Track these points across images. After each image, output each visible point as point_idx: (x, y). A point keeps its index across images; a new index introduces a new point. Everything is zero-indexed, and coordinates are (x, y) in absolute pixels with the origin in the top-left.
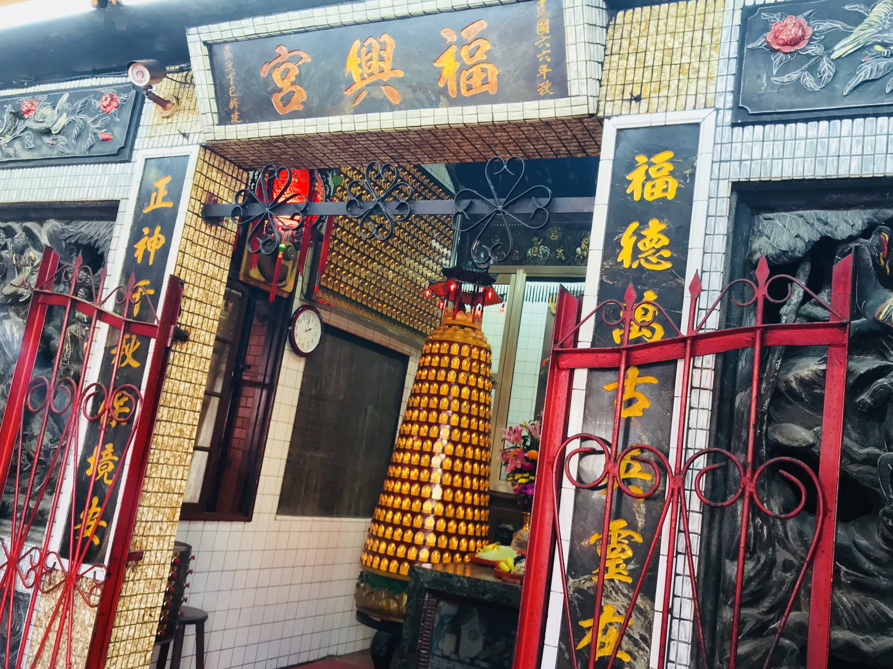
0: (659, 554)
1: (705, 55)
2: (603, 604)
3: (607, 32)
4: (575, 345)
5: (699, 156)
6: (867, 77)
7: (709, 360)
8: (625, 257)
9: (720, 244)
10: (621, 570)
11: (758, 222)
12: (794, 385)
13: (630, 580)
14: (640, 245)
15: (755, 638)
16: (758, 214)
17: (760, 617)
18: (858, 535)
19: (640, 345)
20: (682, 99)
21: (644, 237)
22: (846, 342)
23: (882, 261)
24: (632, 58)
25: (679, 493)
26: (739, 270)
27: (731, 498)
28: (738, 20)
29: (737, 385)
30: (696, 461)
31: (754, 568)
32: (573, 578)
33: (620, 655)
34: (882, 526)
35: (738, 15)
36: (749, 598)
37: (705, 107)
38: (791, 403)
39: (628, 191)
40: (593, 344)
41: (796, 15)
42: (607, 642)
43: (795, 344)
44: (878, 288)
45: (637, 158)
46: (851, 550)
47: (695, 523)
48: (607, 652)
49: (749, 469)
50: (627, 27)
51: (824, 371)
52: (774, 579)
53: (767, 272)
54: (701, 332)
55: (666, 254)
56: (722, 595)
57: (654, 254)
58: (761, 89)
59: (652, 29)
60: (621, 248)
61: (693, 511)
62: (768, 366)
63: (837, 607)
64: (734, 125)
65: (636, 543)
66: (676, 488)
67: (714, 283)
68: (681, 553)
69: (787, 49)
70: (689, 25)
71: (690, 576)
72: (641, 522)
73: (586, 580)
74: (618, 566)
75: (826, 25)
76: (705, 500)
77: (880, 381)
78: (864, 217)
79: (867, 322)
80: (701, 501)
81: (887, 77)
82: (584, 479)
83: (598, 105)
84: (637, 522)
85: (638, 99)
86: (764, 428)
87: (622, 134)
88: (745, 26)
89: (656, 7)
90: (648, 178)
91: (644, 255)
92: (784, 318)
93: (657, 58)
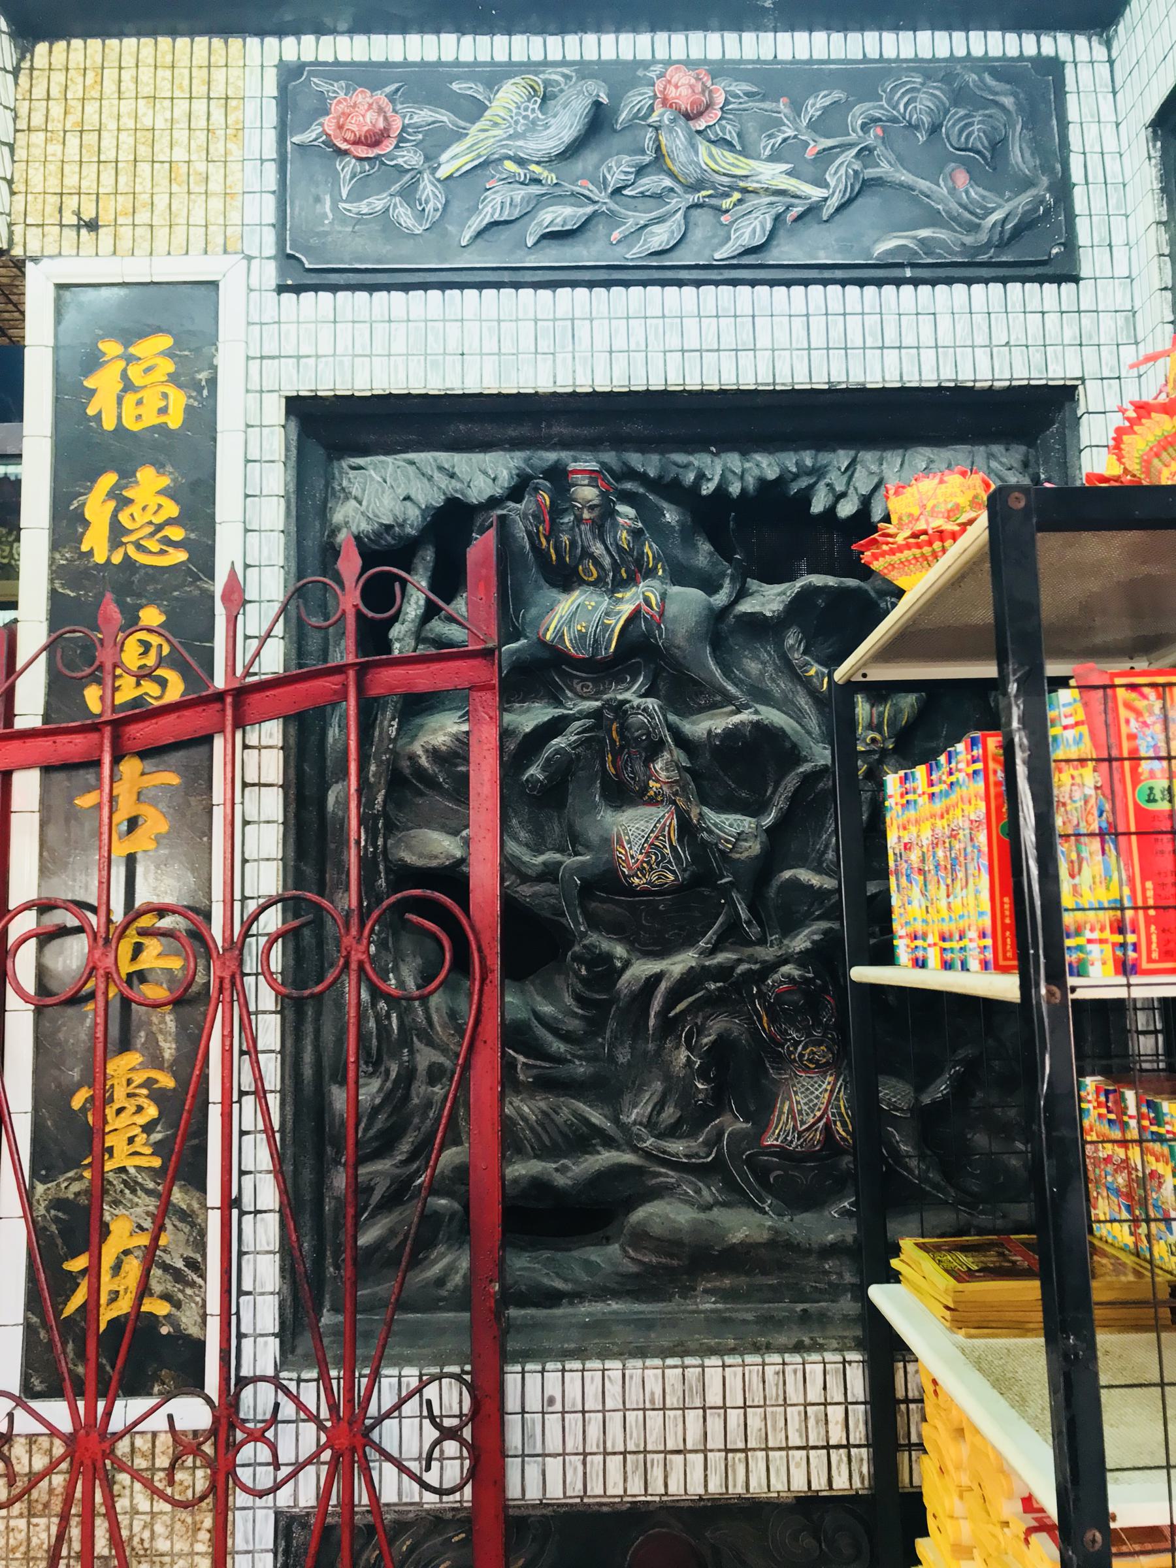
0: (207, 1103)
1: (217, 150)
2: (107, 1217)
3: (16, 84)
4: (9, 722)
5: (220, 345)
6: (496, 217)
7: (272, 732)
8: (96, 542)
9: (273, 514)
10: (138, 1146)
11: (341, 473)
12: (424, 761)
13: (156, 1162)
14: (124, 518)
15: (390, 1211)
16: (339, 459)
17: (398, 1171)
18: (539, 999)
19: (140, 712)
20: (180, 232)
21: (129, 502)
22: (495, 681)
23: (544, 543)
24: (73, 140)
25: (233, 984)
26: (313, 561)
27: (330, 976)
28: (271, 89)
29: (329, 773)
30: (262, 917)
31: (380, 1089)
32: (44, 1182)
33: (148, 1306)
34: (573, 980)
35: (271, 77)
36: (375, 1144)
37: (225, 252)
38: (421, 794)
39: (91, 411)
40: (46, 718)
41: (373, 89)
42: (121, 1289)
43: (416, 690)
44: (541, 588)
45: (101, 346)
46: (530, 1027)
47: (269, 1031)
48: (124, 1306)
49: (354, 921)
50: (58, 78)
51: (467, 733)
52: (416, 1101)
53: (358, 562)
54: (250, 680)
55: (176, 533)
56: (329, 1149)
57: (152, 534)
58: (323, 225)
59: (110, 87)
60: (86, 524)
61: (264, 1012)
62: (377, 733)
63: (515, 1124)
64: (281, 289)
65: (163, 1090)
66: (227, 975)
67: (269, 586)
68: (247, 1093)
69: (362, 151)
70: (181, 87)
71: (265, 1131)
72: (169, 1050)
73: (72, 1180)
74: (131, 1140)
75: (424, 115)
76: (281, 989)
77: (554, 742)
78: (512, 465)
79: (530, 646)
80: (277, 993)
81: (526, 218)
82: (53, 985)
83: (11, 233)
84: (161, 1050)
85: (93, 226)
86: (380, 842)
87: (67, 295)
88: (285, 100)
89: (113, 43)
90: (128, 386)
91: (133, 537)
92: (397, 645)
93: (122, 146)
